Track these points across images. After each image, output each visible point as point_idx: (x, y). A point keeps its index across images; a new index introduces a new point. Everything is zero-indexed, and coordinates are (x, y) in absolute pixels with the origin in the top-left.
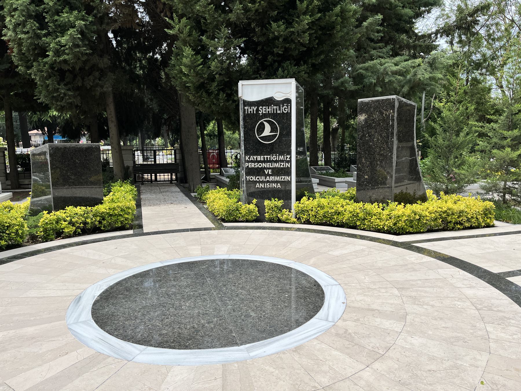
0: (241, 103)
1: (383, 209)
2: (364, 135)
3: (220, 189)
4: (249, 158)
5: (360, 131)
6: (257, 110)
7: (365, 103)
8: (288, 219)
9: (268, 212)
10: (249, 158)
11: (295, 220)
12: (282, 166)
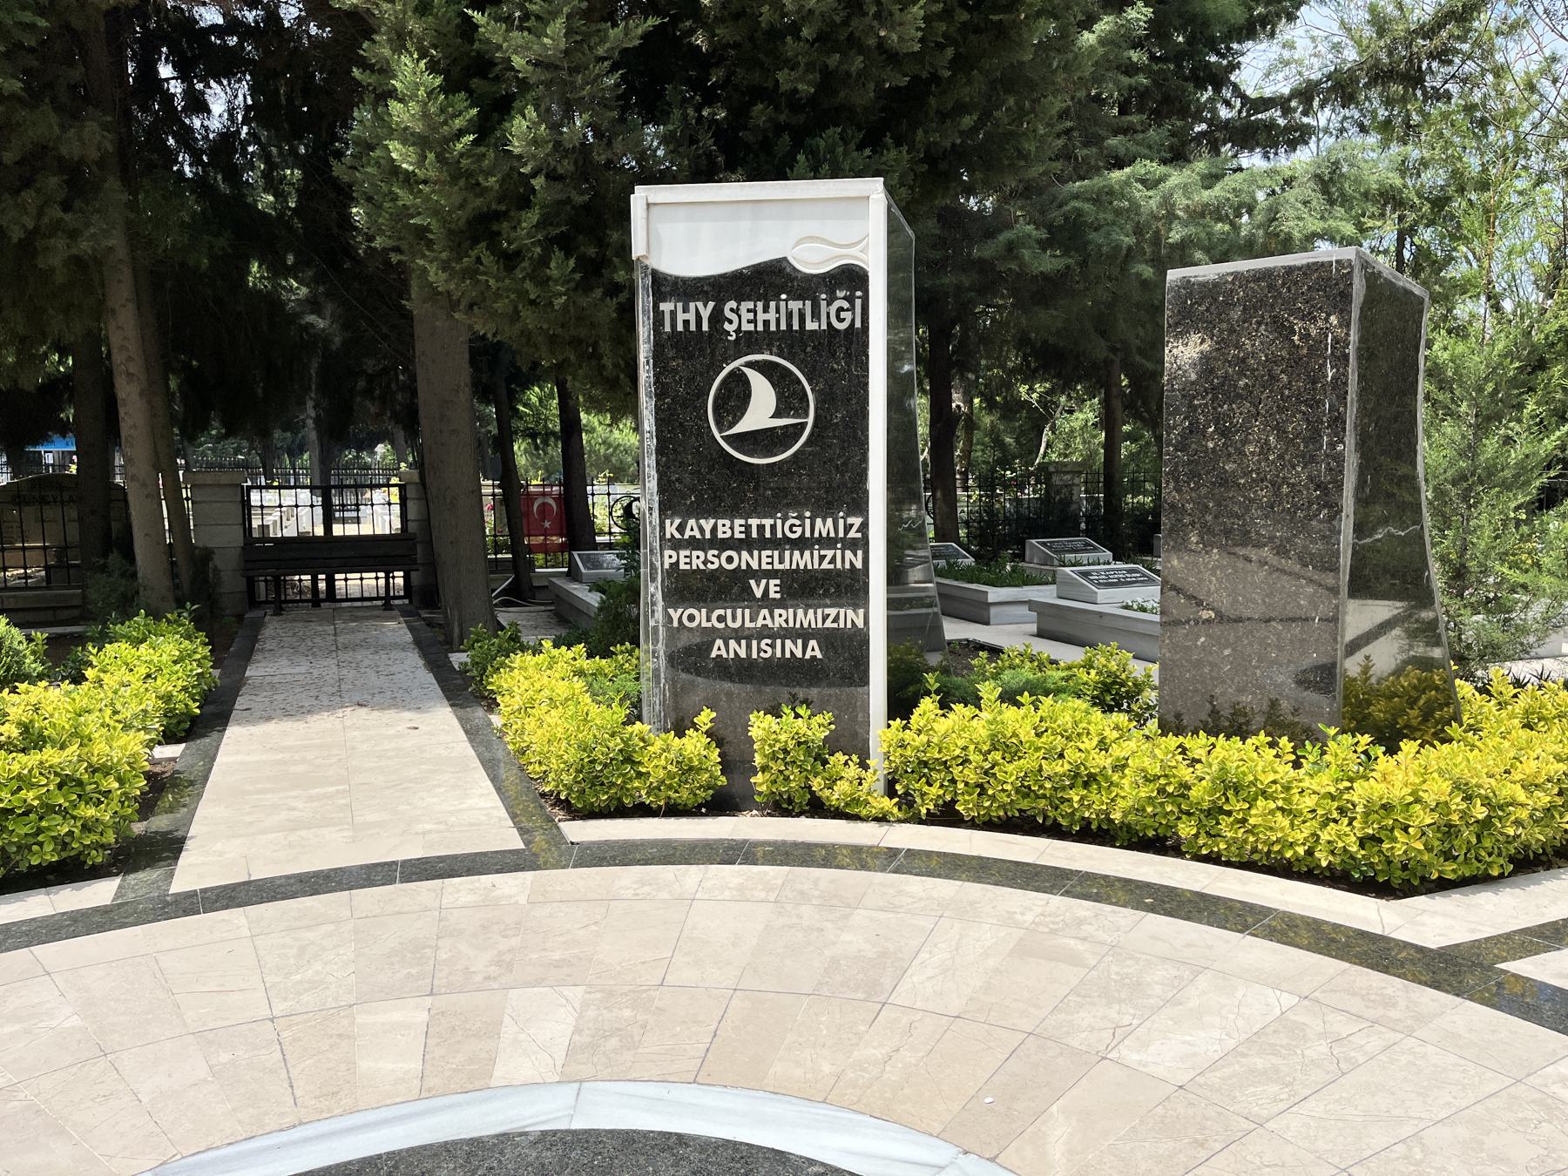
0: (643, 284)
1: (1297, 765)
2: (1195, 429)
3: (555, 652)
4: (681, 529)
5: (1177, 412)
6: (717, 318)
7: (1203, 285)
8: (856, 801)
9: (764, 769)
10: (681, 529)
11: (888, 804)
12: (825, 565)
